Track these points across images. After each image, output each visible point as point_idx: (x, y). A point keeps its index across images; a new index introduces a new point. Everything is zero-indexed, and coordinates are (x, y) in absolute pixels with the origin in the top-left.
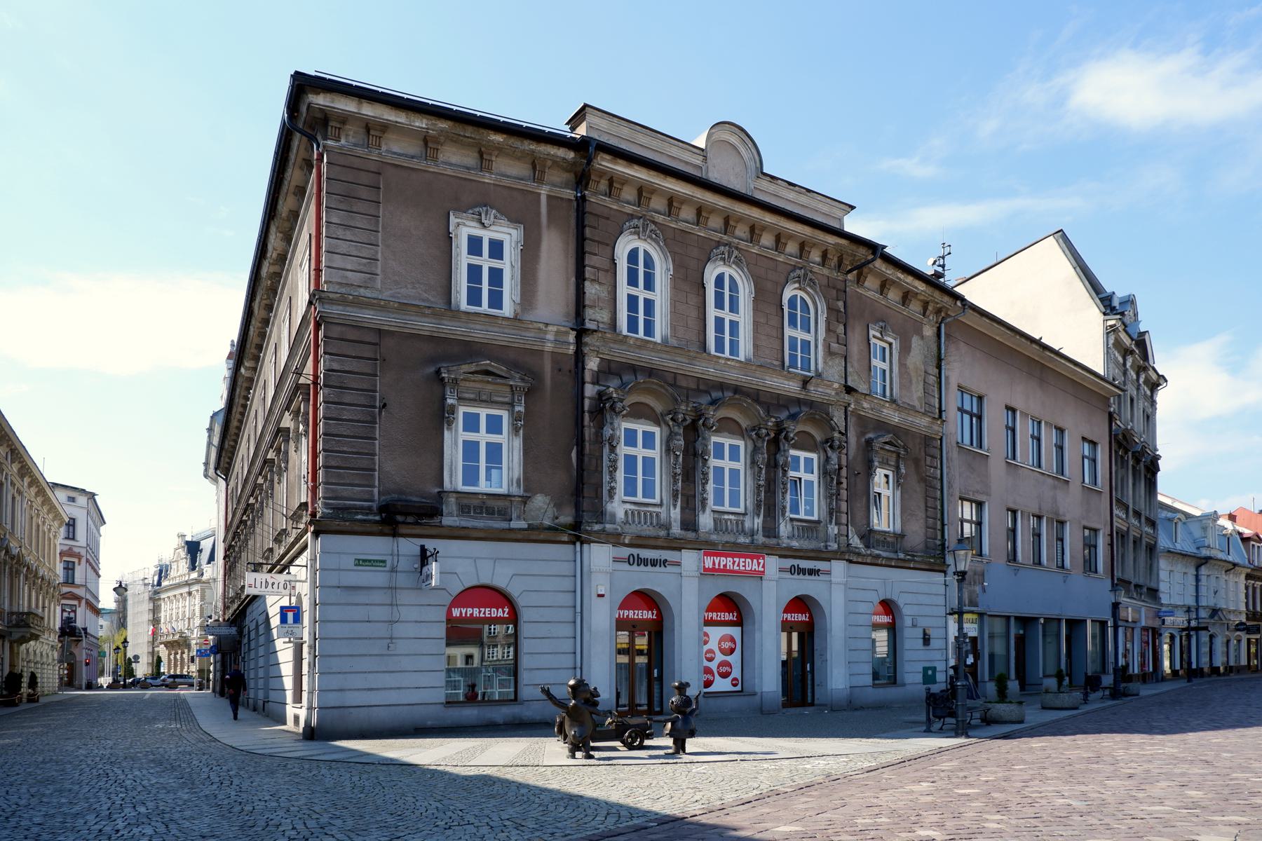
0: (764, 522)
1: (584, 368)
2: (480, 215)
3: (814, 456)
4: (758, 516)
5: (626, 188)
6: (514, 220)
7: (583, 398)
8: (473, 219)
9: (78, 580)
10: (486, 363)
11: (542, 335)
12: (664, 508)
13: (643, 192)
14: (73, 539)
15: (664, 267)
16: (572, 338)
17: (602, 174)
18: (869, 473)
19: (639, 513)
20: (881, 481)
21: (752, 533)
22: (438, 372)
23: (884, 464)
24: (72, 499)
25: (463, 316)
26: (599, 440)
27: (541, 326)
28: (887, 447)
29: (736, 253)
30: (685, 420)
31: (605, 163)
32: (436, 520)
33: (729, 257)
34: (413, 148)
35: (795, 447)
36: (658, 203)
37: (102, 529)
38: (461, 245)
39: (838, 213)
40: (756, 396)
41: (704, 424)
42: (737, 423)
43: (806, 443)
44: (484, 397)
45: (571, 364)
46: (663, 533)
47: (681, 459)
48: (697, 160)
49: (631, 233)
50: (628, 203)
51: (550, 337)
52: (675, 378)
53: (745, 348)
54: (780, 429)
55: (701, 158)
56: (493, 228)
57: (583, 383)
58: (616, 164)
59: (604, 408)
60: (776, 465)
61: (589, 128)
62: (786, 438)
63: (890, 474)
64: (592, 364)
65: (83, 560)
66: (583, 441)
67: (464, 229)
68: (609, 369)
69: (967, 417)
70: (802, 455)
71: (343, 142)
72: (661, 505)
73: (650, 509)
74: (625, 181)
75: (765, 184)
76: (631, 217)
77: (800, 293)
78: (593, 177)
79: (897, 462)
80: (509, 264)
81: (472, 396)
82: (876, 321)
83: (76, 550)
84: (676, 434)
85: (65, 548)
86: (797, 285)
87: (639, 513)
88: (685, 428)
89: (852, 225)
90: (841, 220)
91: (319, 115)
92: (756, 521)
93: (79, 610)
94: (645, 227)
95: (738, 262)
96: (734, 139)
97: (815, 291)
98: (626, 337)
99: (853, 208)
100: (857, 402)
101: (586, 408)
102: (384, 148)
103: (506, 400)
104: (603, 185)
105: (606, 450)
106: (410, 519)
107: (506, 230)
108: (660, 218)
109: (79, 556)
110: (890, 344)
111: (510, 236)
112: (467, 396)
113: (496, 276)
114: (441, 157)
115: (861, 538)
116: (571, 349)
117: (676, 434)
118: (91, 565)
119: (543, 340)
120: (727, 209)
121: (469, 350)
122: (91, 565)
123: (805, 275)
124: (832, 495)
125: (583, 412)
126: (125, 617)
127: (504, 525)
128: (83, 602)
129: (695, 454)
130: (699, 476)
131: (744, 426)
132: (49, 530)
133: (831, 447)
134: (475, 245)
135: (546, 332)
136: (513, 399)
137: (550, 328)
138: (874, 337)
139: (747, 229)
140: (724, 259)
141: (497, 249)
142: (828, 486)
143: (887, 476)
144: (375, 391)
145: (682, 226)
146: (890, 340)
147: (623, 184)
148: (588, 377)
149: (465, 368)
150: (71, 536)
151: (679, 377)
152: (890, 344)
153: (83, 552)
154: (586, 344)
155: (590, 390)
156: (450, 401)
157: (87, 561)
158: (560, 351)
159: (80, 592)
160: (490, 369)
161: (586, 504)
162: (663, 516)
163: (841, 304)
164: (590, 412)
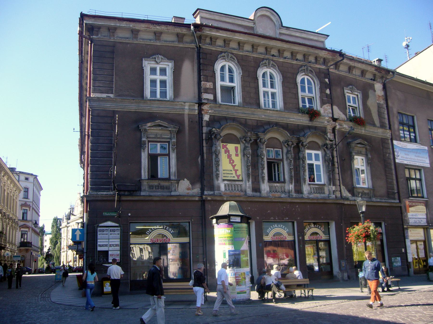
0: (295, 186)
1: (202, 120)
2: (155, 58)
3: (319, 152)
4: (292, 183)
5: (217, 41)
6: (169, 58)
7: (202, 133)
8: (153, 61)
9: (29, 218)
10: (158, 122)
11: (183, 107)
12: (244, 182)
13: (226, 42)
14: (27, 198)
15: (238, 72)
16: (196, 107)
17: (206, 36)
18: (351, 159)
19: (231, 185)
20: (359, 162)
21: (289, 192)
22: (138, 127)
23: (359, 153)
24: (27, 179)
25: (148, 102)
26: (210, 152)
27: (183, 103)
28: (359, 145)
29: (271, 62)
30: (250, 140)
31: (207, 32)
32: (138, 193)
33: (269, 65)
34: (127, 34)
35: (309, 148)
36: (233, 45)
37: (42, 192)
38: (147, 71)
39: (322, 40)
40: (286, 127)
41: (260, 141)
42: (277, 139)
43: (314, 146)
44: (159, 136)
45: (197, 119)
46: (242, 194)
47: (250, 158)
48: (251, 25)
49: (222, 59)
50: (220, 46)
51: (187, 107)
52: (246, 121)
53: (280, 104)
54: (299, 141)
55: (253, 23)
56: (161, 63)
57: (202, 127)
58: (212, 31)
59: (212, 138)
60: (299, 158)
61: (202, 18)
62: (302, 145)
63: (364, 158)
64: (206, 118)
65: (31, 208)
66: (203, 153)
67: (147, 65)
68: (214, 120)
70: (313, 152)
71: (99, 36)
72: (242, 181)
73: (237, 183)
74: (217, 38)
75: (284, 31)
76: (221, 52)
77: (306, 77)
78: (202, 38)
79: (366, 152)
80: (169, 78)
81: (153, 136)
82: (347, 86)
83: (28, 203)
84: (247, 147)
85: (23, 203)
86: (304, 74)
87: (231, 185)
88: (251, 144)
89: (330, 44)
90: (323, 42)
91: (90, 27)
92: (291, 186)
93: (29, 233)
94: (228, 55)
95: (273, 66)
96: (268, 14)
97: (313, 75)
98: (221, 104)
99: (328, 36)
100: (340, 125)
101: (204, 138)
102: (116, 36)
103: (168, 137)
104: (208, 40)
105: (214, 157)
106: (126, 193)
107: (166, 63)
108: (235, 52)
109: (29, 206)
110: (357, 95)
111: (169, 66)
112: (151, 136)
113: (164, 83)
114: (139, 37)
115: (349, 191)
116: (196, 112)
117: (247, 147)
118: (35, 210)
119: (183, 109)
120: (265, 46)
121: (152, 117)
122: (35, 210)
123: (307, 69)
124: (330, 172)
125: (203, 140)
126: (239, 201)
127: (168, 194)
128: (31, 229)
129: (258, 156)
130: (260, 166)
131: (281, 140)
132: (14, 195)
133: (327, 148)
134: (153, 71)
135: (185, 106)
136: (171, 136)
137: (186, 104)
138: (347, 93)
139: (277, 51)
140: (266, 66)
141: (163, 71)
142: (328, 167)
143: (362, 159)
144: (112, 137)
145: (246, 54)
146: (356, 93)
147: (216, 39)
148: (204, 124)
149: (149, 124)
150: (26, 197)
151: (247, 120)
152: (357, 95)
153: (31, 204)
154: (203, 110)
155: (205, 130)
156: (143, 139)
157: (33, 208)
158: (192, 113)
159: (30, 224)
160: (160, 124)
161: (205, 183)
162: (243, 186)
163: (327, 80)
164: (206, 140)
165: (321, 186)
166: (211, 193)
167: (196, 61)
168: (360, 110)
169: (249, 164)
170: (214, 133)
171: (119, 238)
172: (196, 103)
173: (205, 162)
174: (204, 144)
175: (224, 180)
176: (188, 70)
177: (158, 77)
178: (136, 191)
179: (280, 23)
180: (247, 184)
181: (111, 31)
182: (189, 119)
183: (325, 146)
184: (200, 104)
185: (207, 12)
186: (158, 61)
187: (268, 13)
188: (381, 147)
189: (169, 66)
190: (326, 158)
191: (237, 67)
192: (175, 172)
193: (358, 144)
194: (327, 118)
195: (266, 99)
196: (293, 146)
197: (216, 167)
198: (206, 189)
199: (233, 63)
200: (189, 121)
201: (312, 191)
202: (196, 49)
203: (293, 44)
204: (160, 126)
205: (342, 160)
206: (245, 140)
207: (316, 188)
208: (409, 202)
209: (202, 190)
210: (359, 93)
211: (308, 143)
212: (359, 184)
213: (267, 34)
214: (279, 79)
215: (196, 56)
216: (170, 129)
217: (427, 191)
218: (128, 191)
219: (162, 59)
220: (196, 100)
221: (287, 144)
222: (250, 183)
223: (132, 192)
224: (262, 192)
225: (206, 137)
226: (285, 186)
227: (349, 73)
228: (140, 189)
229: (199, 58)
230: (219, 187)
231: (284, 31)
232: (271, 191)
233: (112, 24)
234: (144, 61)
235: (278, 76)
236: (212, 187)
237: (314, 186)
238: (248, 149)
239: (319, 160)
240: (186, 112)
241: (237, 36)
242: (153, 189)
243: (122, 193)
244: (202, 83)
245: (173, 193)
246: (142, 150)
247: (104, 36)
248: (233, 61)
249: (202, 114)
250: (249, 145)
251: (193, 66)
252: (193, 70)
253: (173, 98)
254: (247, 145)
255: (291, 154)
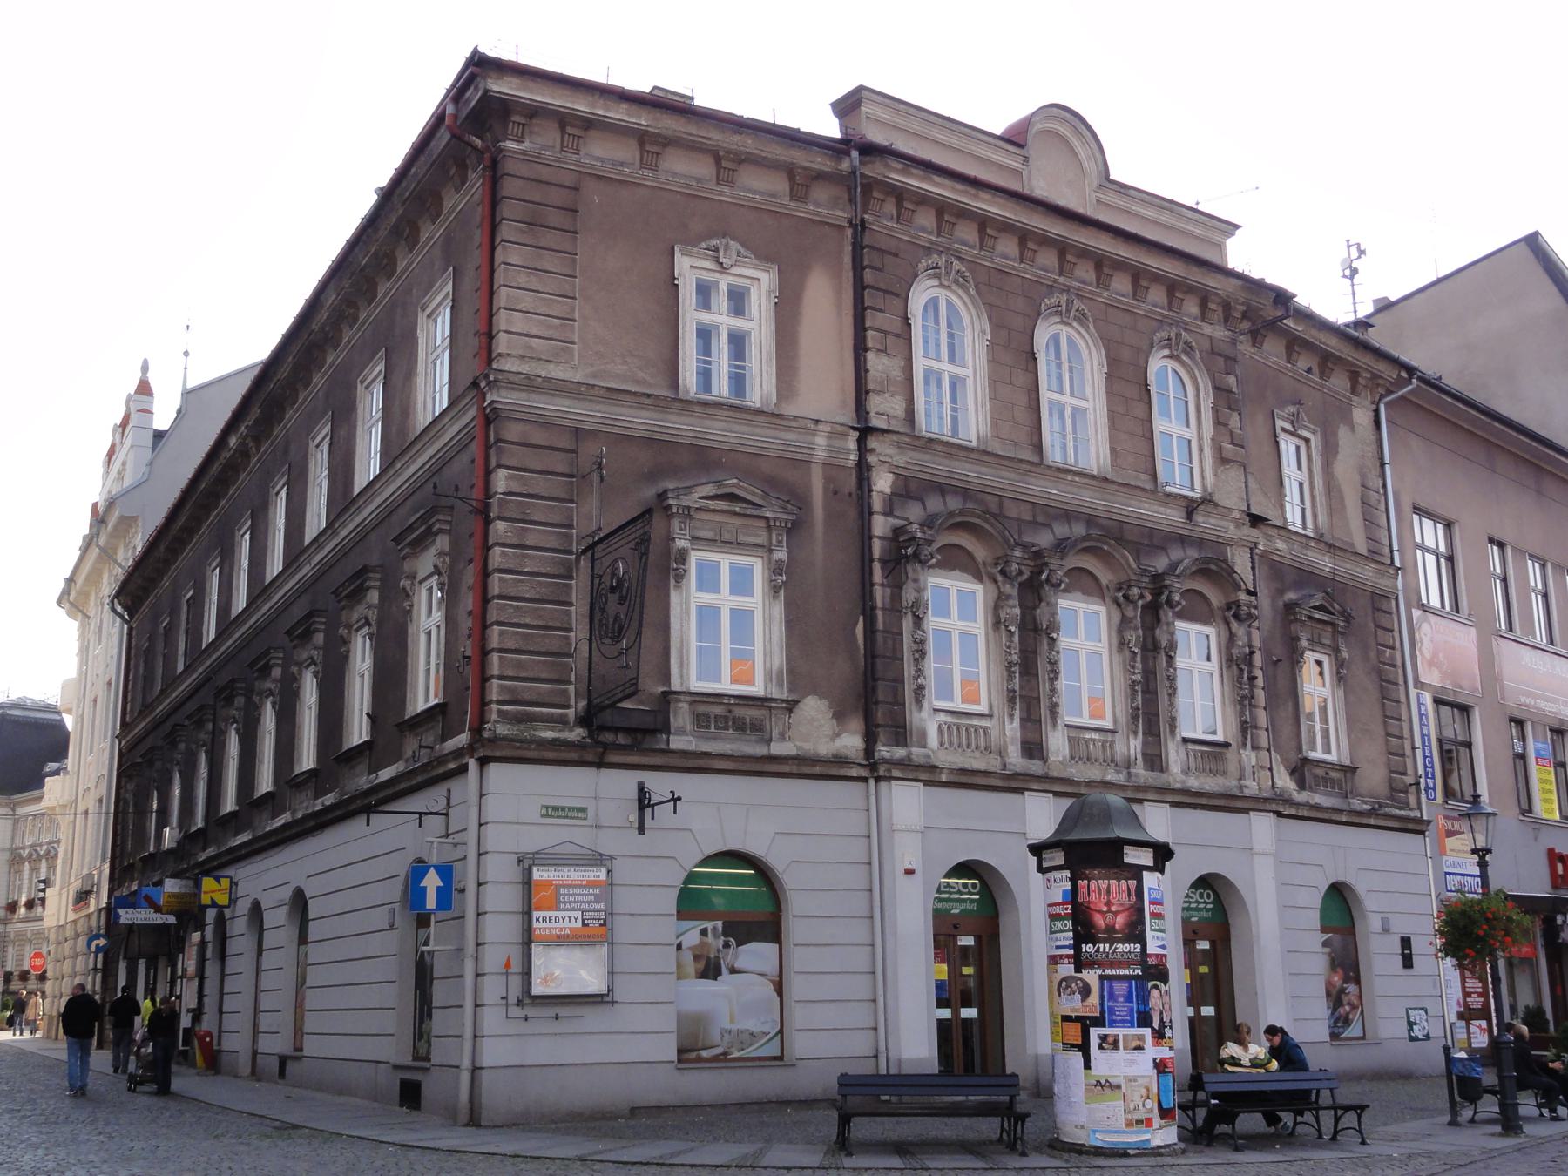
0: (1145, 744)
1: (870, 491)
2: (717, 250)
6: (765, 256)
8: (706, 258)
12: (995, 720)
16: (852, 444)
26: (895, 608)
42: (1091, 574)
56: (735, 270)
57: (871, 514)
60: (1156, 648)
64: (883, 483)
69: (1430, 559)
73: (975, 722)
75: (1110, 198)
80: (759, 323)
84: (1009, 597)
86: (1166, 352)
88: (1020, 584)
89: (1241, 256)
90: (1220, 247)
92: (1132, 742)
99: (1237, 227)
105: (907, 623)
106: (622, 739)
117: (1009, 597)
125: (872, 560)
137: (821, 427)
140: (1059, 313)
141: (738, 302)
143: (1319, 663)
148: (877, 504)
151: (1007, 503)
155: (880, 526)
156: (681, 543)
160: (737, 492)
161: (880, 715)
162: (994, 734)
164: (883, 562)
165: (1217, 750)
166: (900, 752)
167: (848, 275)
168: (1317, 492)
169: (1015, 658)
170: (914, 538)
171: (265, 915)
172: (854, 428)
173: (880, 637)
174: (878, 576)
175: (936, 710)
176: (825, 303)
177: (722, 319)
178: (653, 732)
179: (1101, 168)
180: (1008, 726)
181: (569, 130)
182: (828, 480)
183: (1229, 608)
184: (865, 432)
185: (887, 101)
186: (726, 261)
187: (1061, 129)
188: (1372, 625)
189: (762, 284)
190: (1235, 651)
191: (973, 312)
192: (780, 672)
193: (1315, 608)
194: (1236, 515)
195: (934, 398)
196: (1140, 603)
197: (916, 660)
198: (882, 737)
199: (960, 292)
200: (825, 489)
201: (1192, 764)
202: (849, 232)
203: (1094, 230)
204: (732, 497)
205: (1272, 664)
206: (1002, 572)
207: (1203, 752)
208: (1446, 817)
209: (870, 739)
210: (1314, 432)
211: (939, 550)
212: (1314, 749)
213: (1062, 202)
214: (1096, 362)
215: (847, 259)
216: (768, 514)
217: (1490, 784)
218: (628, 731)
219: (739, 253)
220: (848, 416)
221: (1125, 596)
222: (1017, 723)
223: (639, 736)
224: (1052, 758)
225: (883, 551)
226: (1112, 742)
227: (1134, 297)
228: (666, 728)
229: (858, 267)
230: (923, 735)
231: (1110, 198)
232: (1073, 758)
233: (581, 105)
234: (677, 255)
235: (1094, 354)
236: (901, 733)
237: (1197, 747)
238: (1011, 602)
239: (749, 592)
240: (820, 454)
241: (984, 201)
242: (708, 727)
243: (608, 737)
244: (870, 356)
245: (777, 749)
246: (672, 582)
247: (543, 147)
248: (961, 286)
249: (869, 468)
250: (1015, 592)
251: (839, 292)
252: (839, 306)
253: (774, 399)
254: (1008, 589)
255: (1136, 629)
